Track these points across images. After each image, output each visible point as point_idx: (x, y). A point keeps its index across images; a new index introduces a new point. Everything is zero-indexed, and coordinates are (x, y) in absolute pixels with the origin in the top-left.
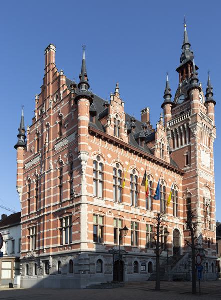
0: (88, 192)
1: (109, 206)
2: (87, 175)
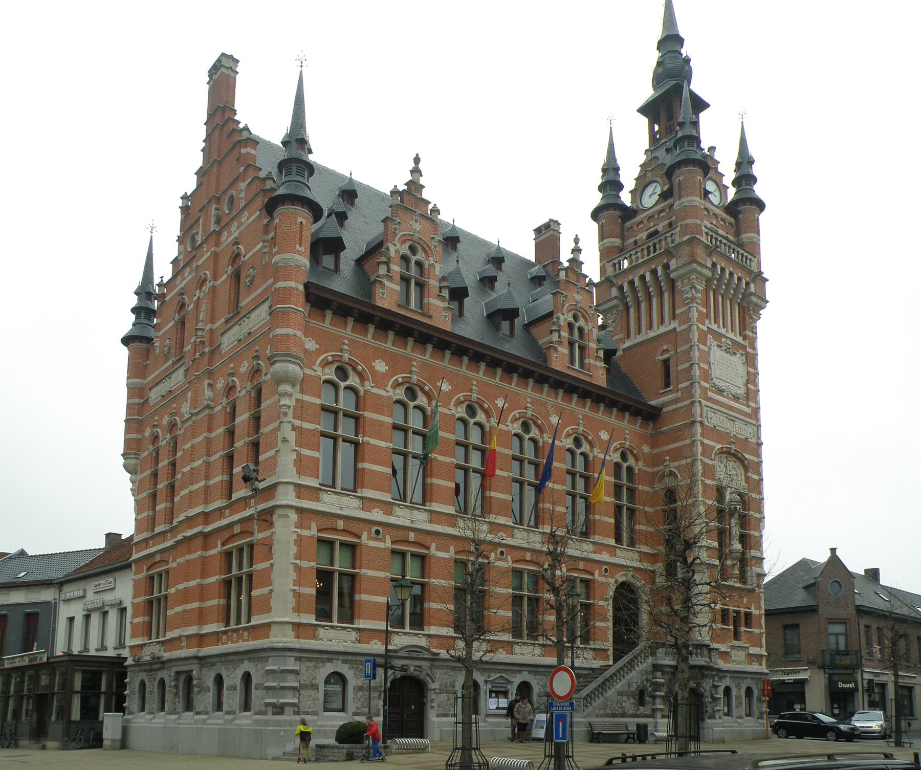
0: (299, 473)
2: (297, 423)
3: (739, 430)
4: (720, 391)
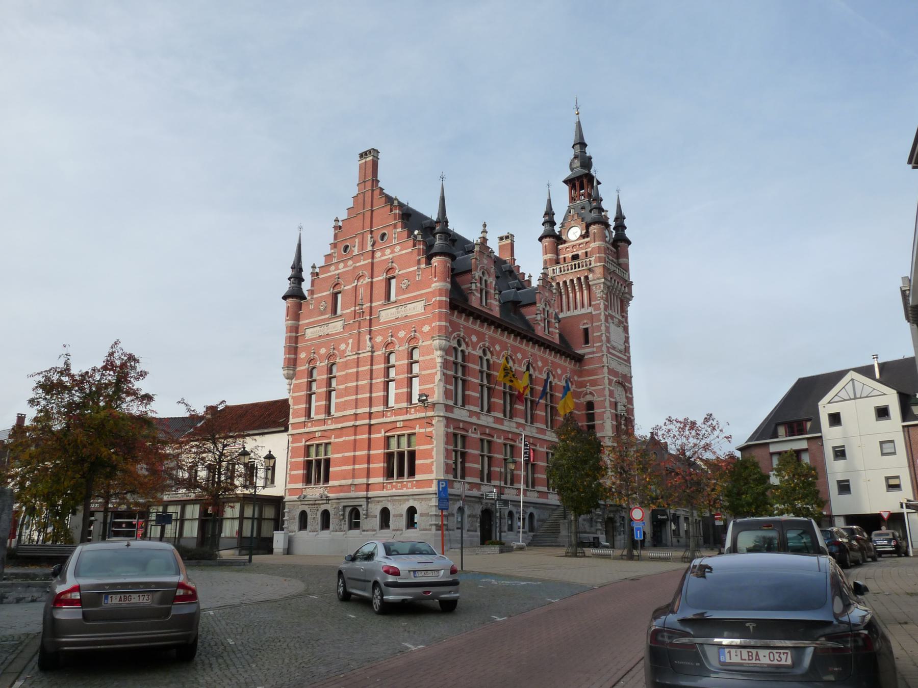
1: (474, 420)
3: (621, 369)
4: (614, 348)
